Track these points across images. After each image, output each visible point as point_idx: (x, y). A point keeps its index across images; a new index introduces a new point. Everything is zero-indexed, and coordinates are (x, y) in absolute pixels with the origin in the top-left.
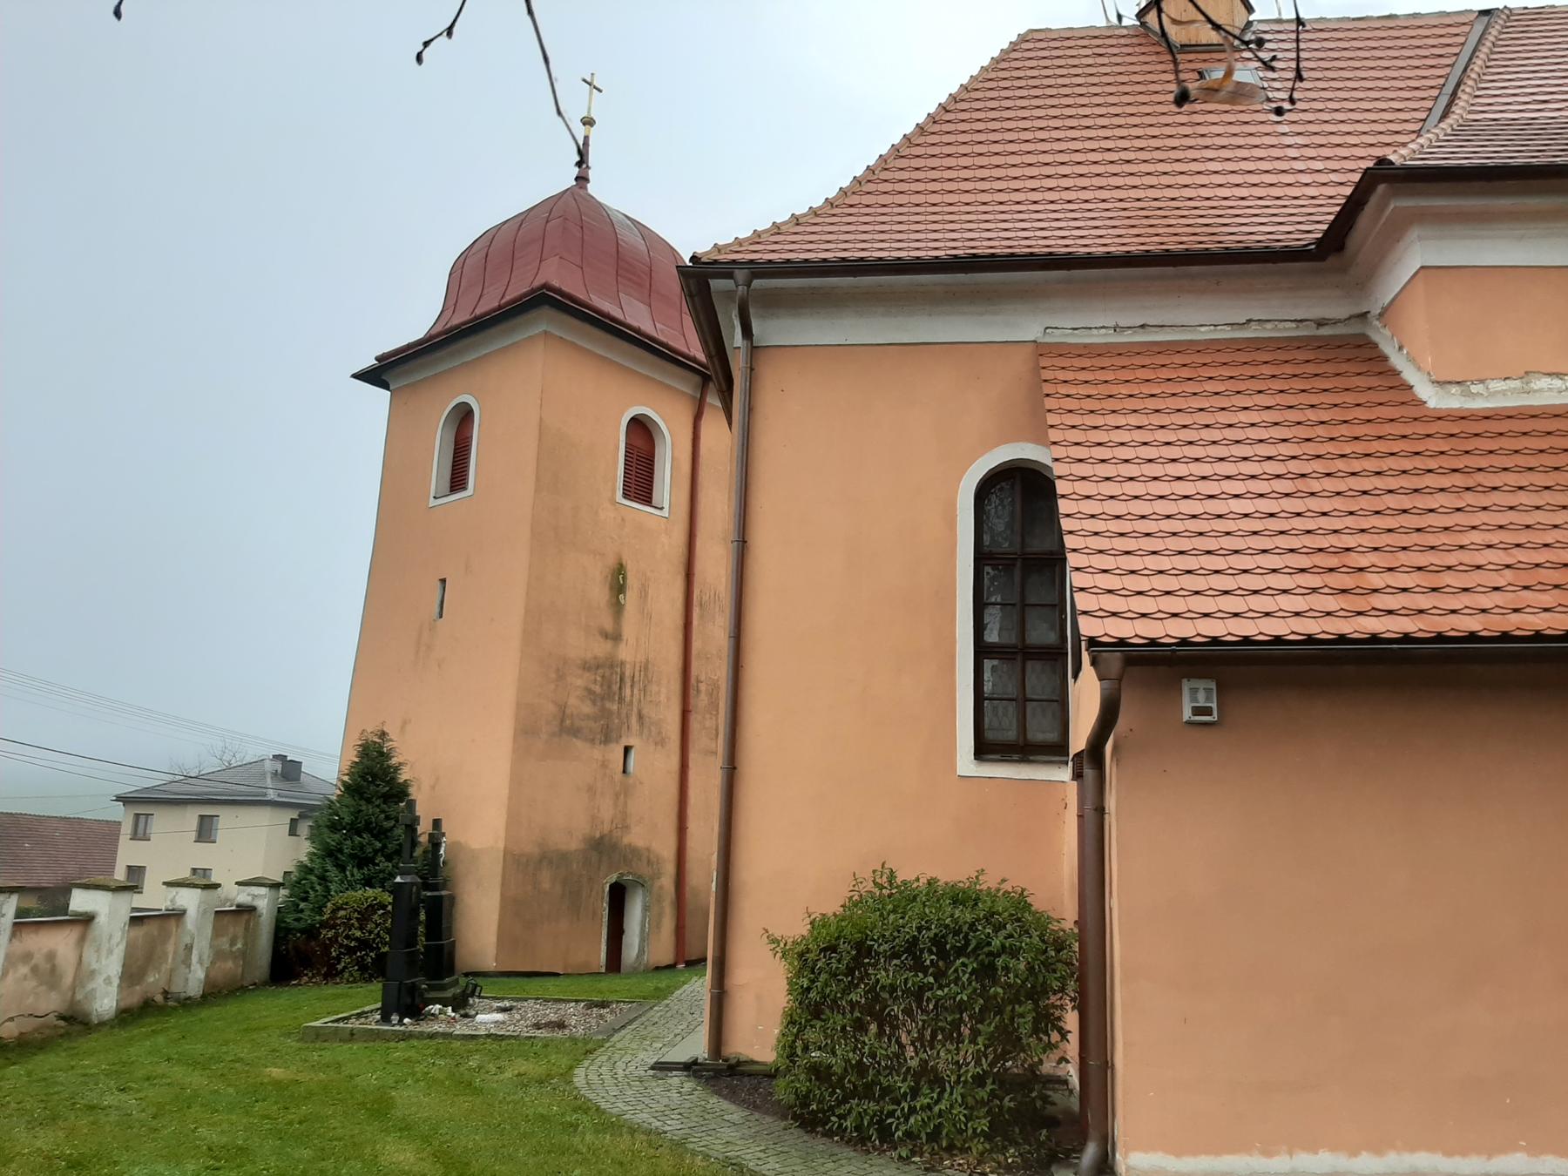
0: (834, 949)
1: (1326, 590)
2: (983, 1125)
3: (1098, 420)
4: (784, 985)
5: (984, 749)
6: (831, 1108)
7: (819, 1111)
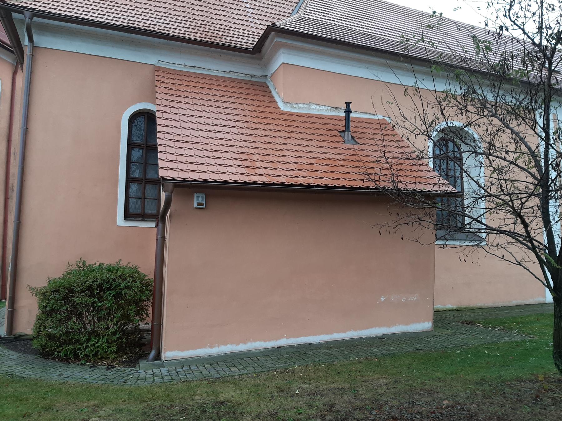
0: (57, 291)
1: (243, 166)
2: (114, 349)
3: (174, 98)
4: (37, 305)
5: (128, 216)
6: (55, 349)
7: (50, 351)
